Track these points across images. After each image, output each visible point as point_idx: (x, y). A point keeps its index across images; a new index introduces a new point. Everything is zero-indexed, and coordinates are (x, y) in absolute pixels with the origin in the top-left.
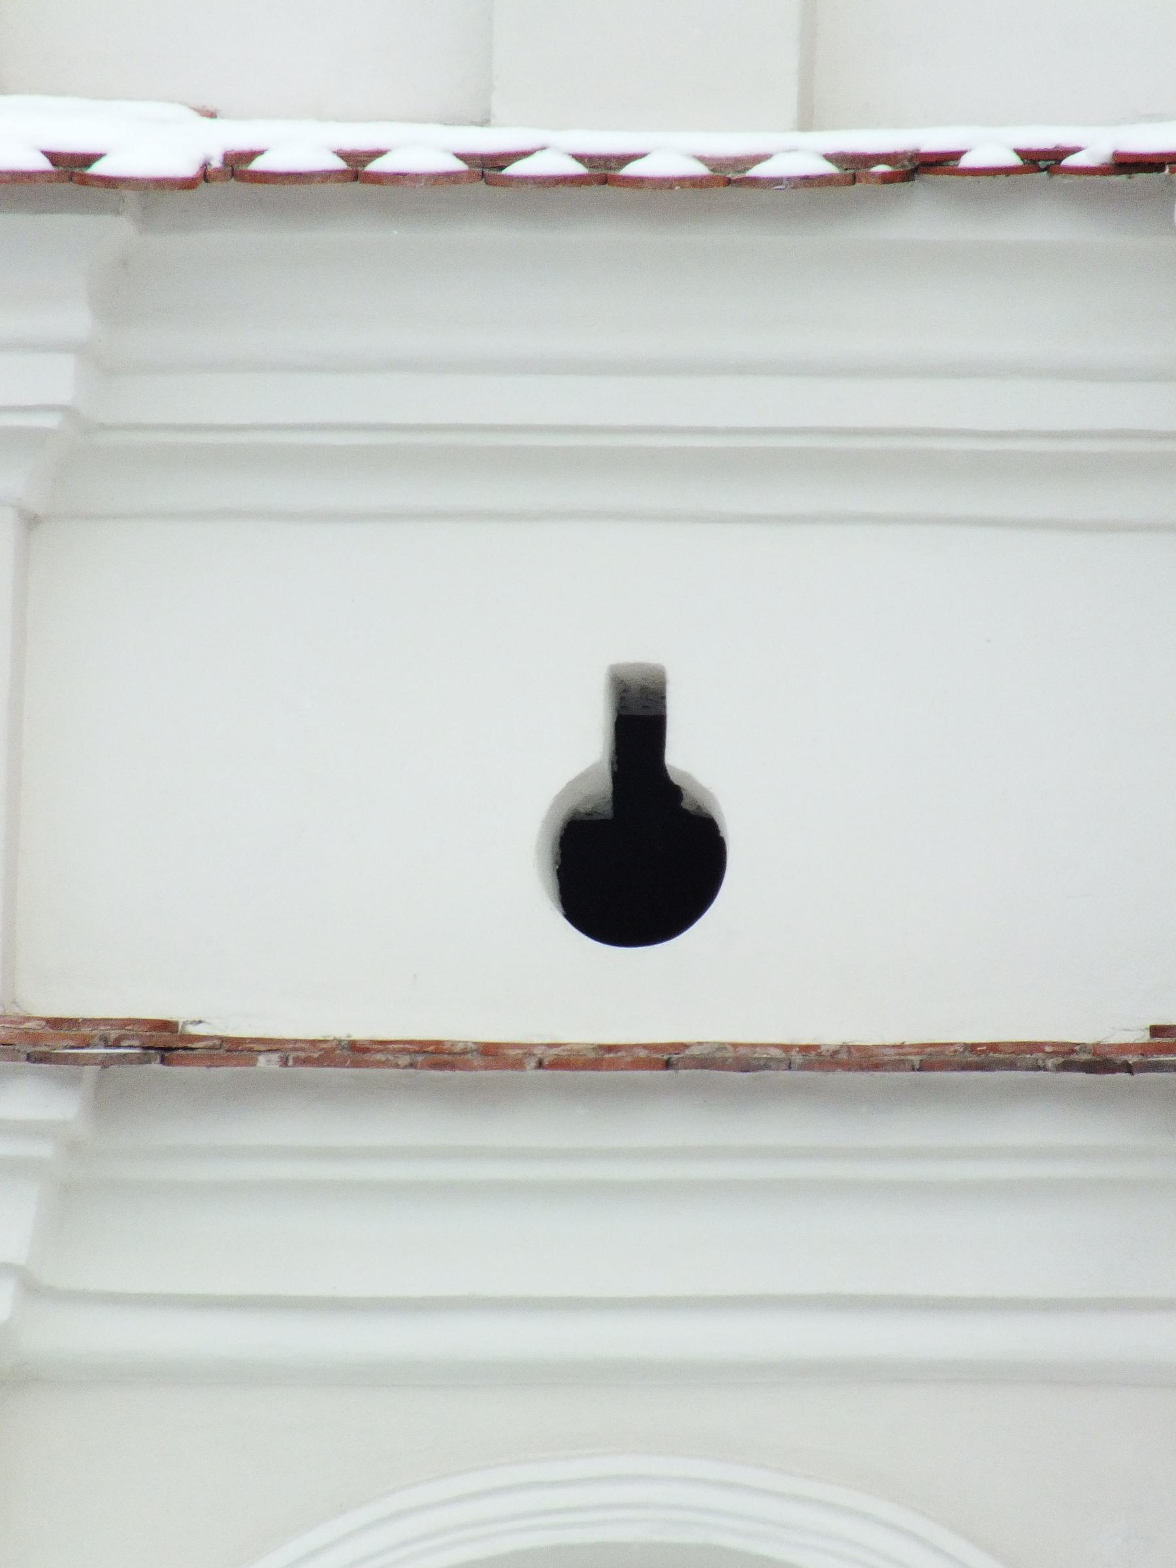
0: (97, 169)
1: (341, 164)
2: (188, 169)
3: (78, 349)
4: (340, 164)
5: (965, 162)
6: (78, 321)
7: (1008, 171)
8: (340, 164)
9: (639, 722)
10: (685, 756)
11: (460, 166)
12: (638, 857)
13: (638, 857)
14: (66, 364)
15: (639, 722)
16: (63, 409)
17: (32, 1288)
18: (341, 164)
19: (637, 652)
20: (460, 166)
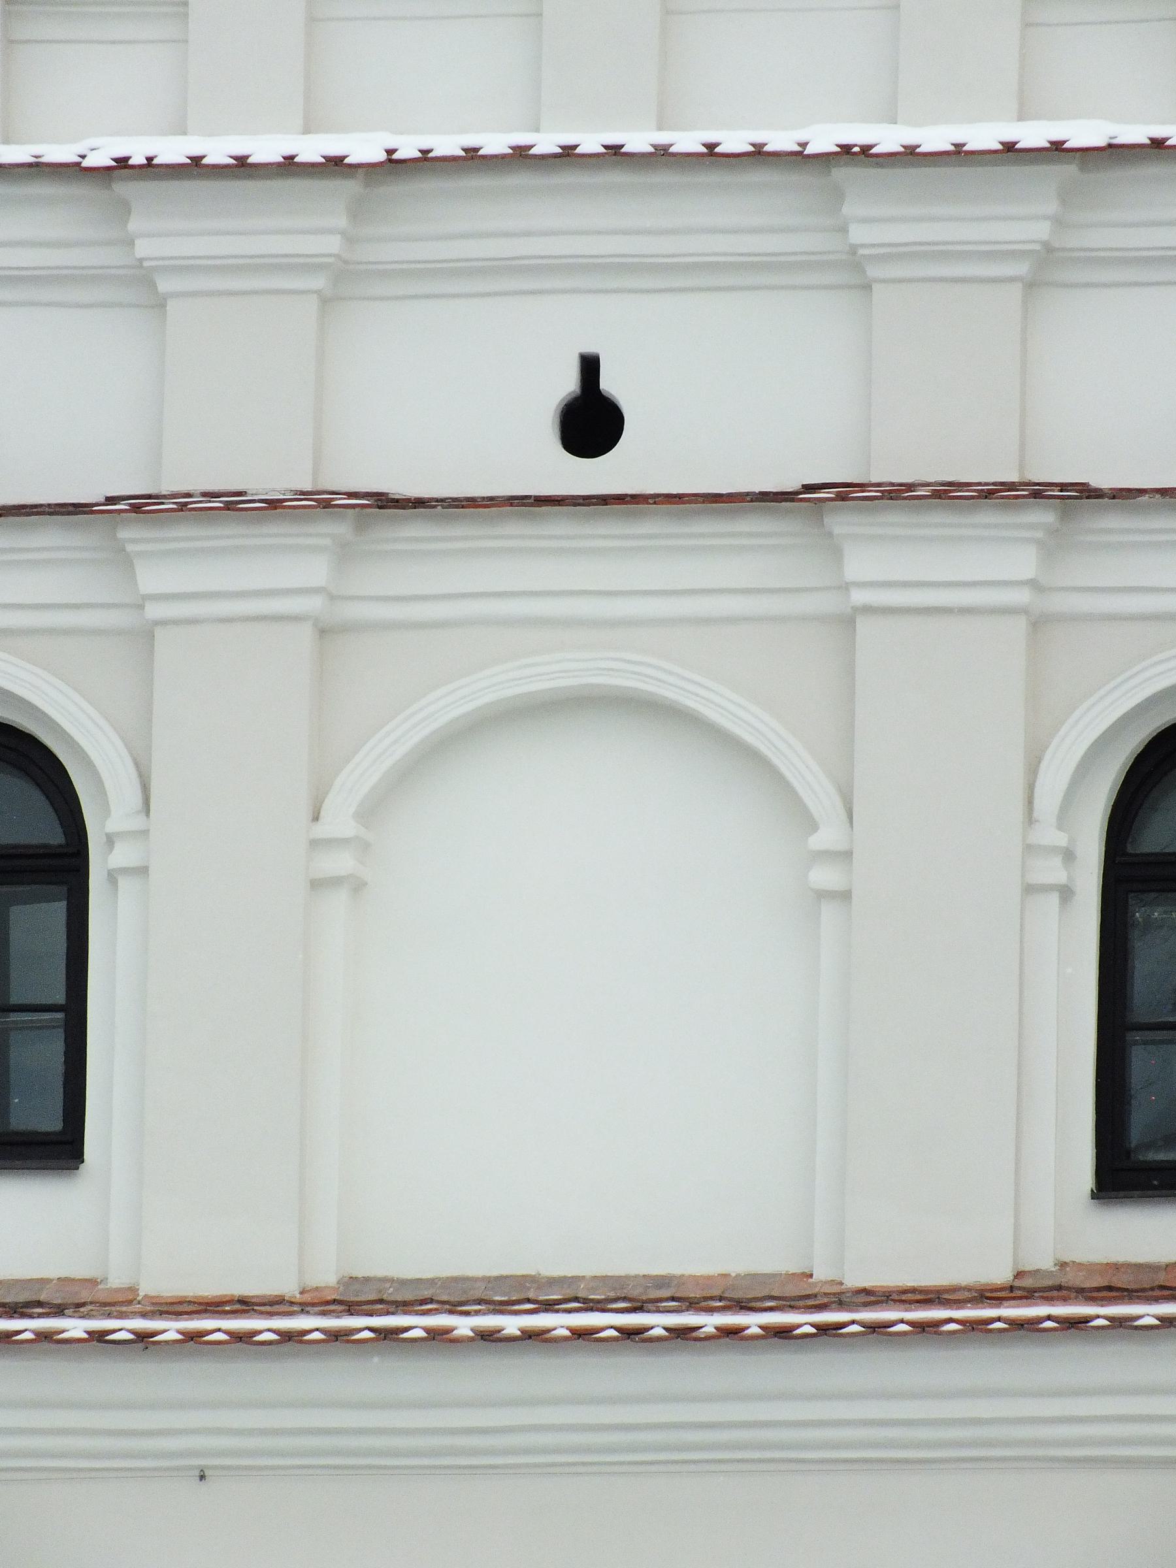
0: (578, 151)
1: (752, 149)
2: (1101, 142)
3: (343, 233)
4: (952, 148)
5: (131, 162)
6: (342, 222)
7: (996, 152)
8: (952, 148)
9: (590, 367)
10: (607, 384)
11: (838, 149)
12: (591, 422)
13: (591, 422)
14: (339, 236)
15: (590, 367)
16: (334, 255)
17: (332, 598)
18: (704, 150)
19: (590, 349)
20: (838, 149)
